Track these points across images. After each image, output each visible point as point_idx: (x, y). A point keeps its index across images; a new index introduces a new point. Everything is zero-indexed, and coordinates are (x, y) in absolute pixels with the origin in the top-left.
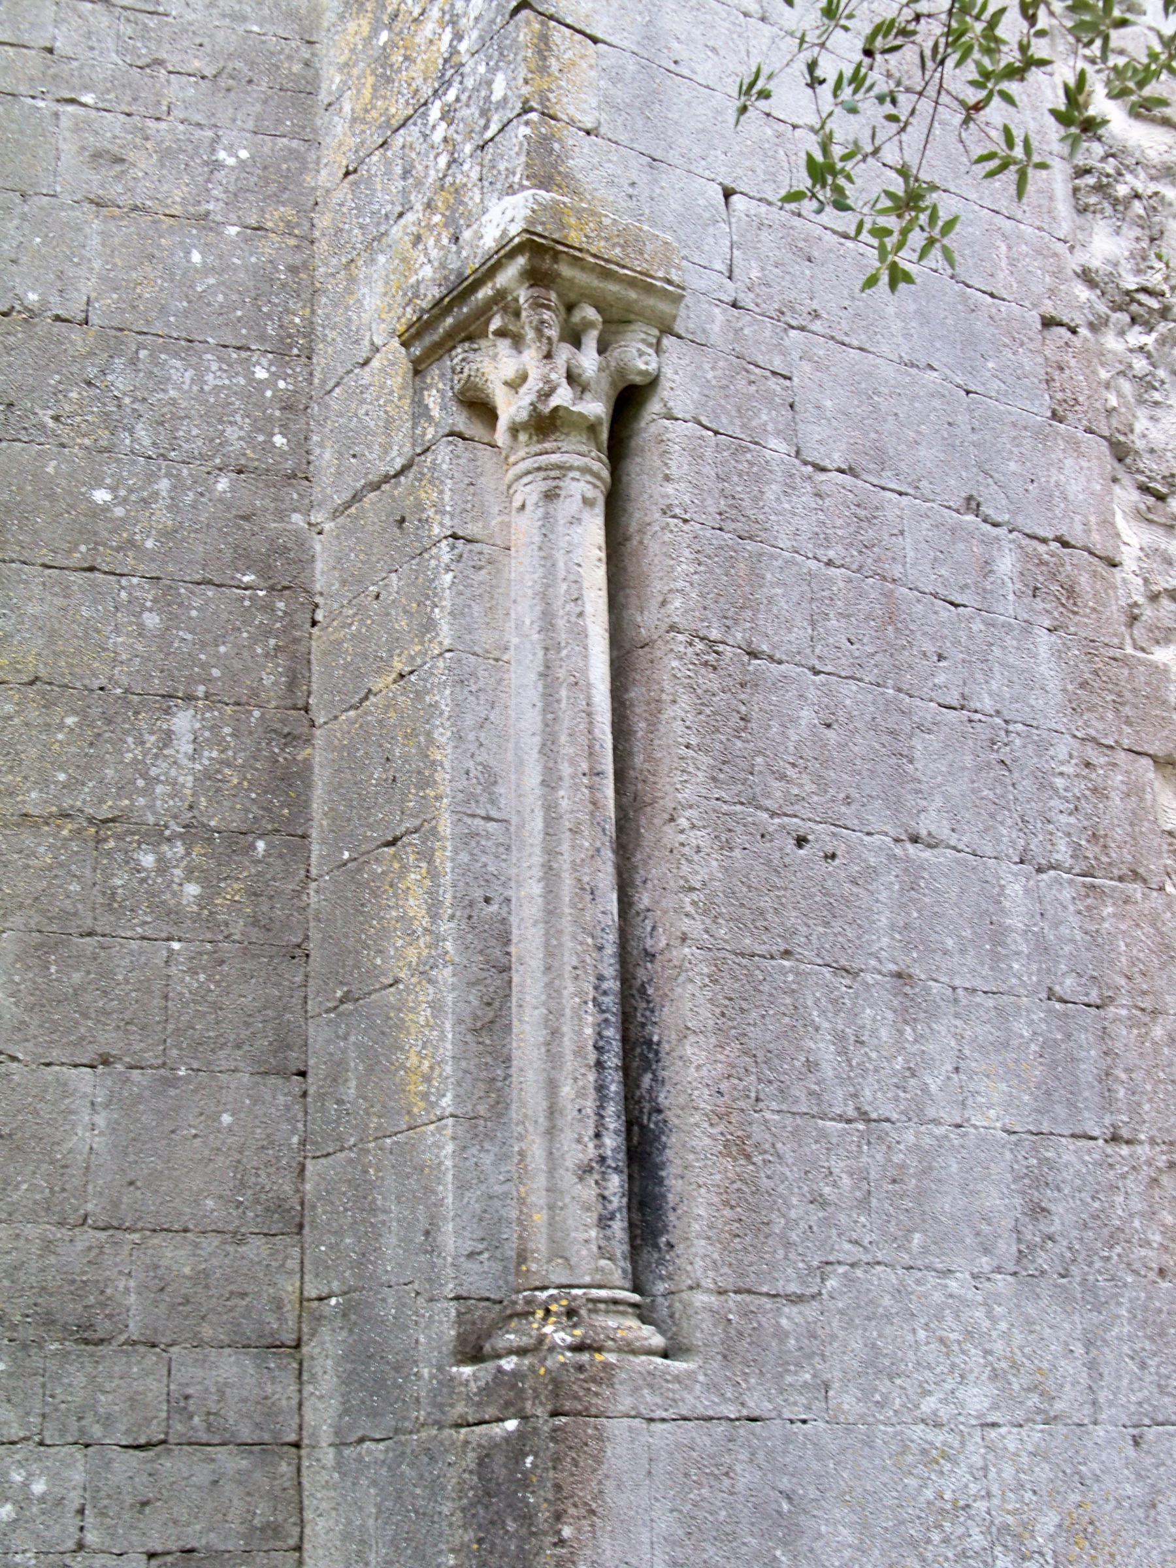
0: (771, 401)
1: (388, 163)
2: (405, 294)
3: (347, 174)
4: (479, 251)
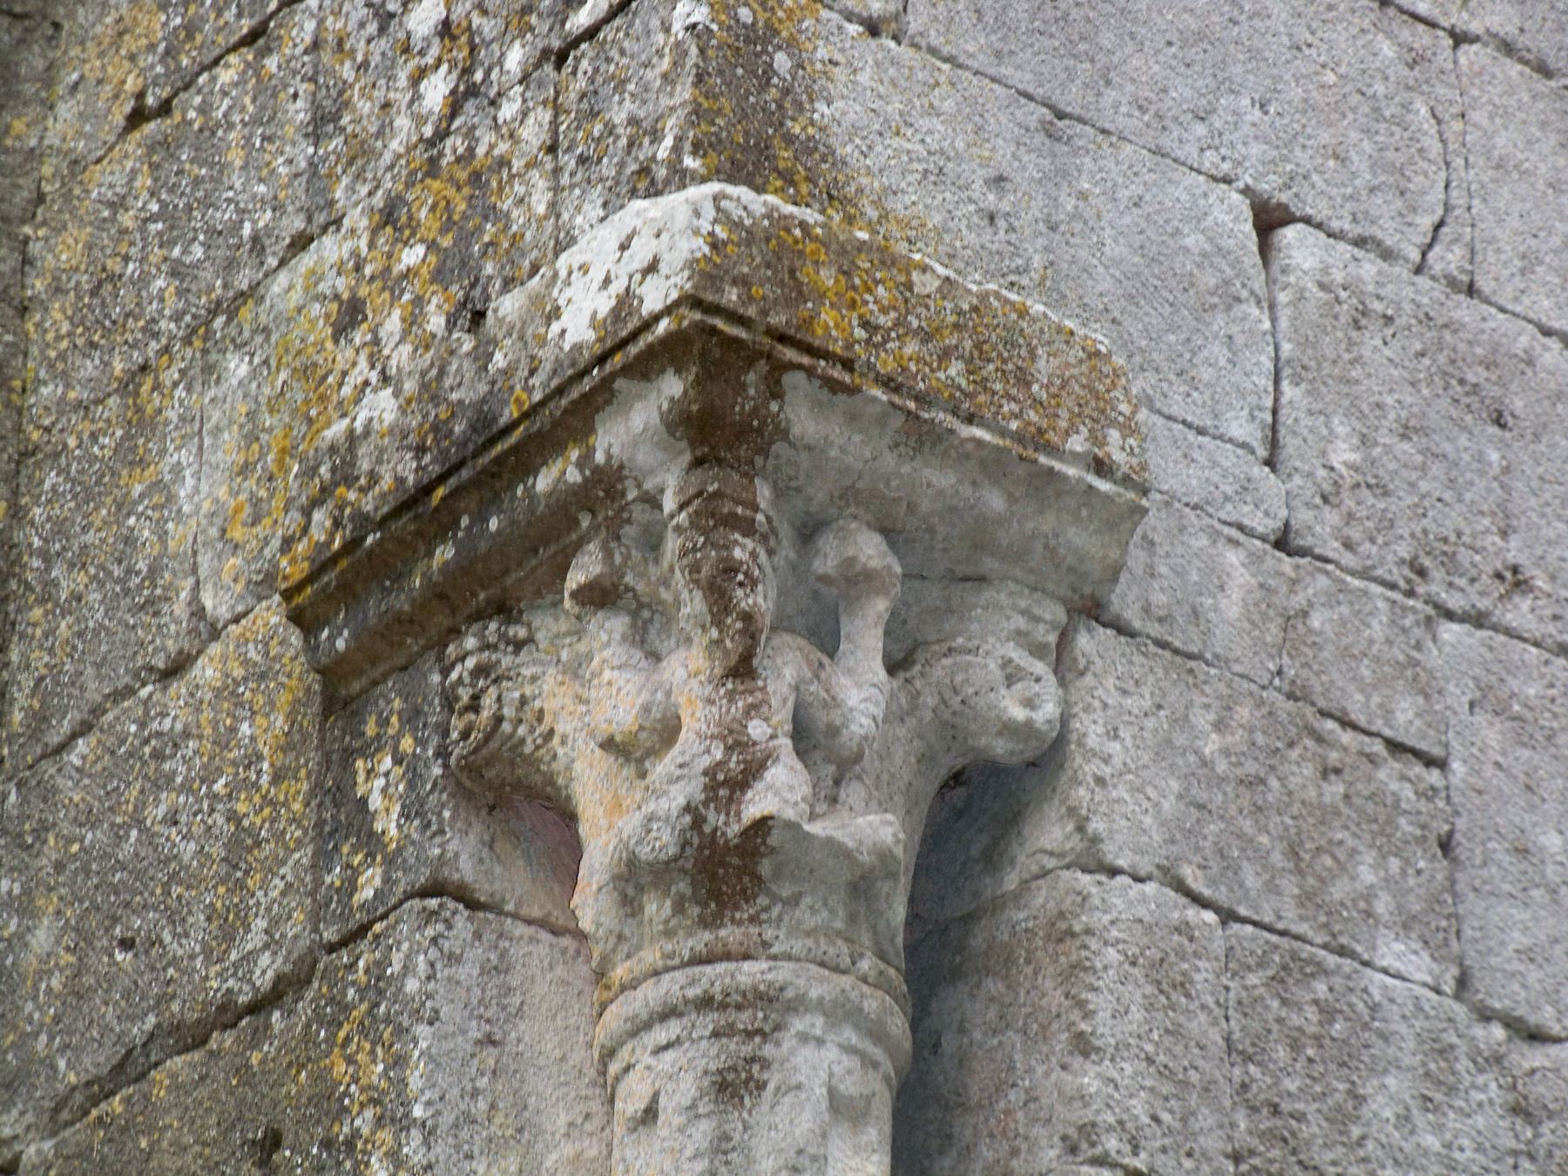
0: (1386, 829)
1: (267, 91)
2: (311, 472)
3: (137, 117)
4: (547, 355)
